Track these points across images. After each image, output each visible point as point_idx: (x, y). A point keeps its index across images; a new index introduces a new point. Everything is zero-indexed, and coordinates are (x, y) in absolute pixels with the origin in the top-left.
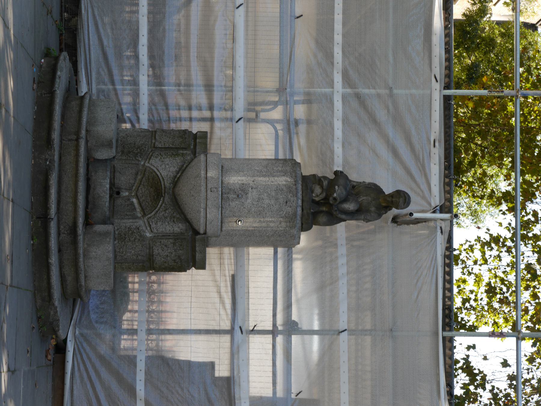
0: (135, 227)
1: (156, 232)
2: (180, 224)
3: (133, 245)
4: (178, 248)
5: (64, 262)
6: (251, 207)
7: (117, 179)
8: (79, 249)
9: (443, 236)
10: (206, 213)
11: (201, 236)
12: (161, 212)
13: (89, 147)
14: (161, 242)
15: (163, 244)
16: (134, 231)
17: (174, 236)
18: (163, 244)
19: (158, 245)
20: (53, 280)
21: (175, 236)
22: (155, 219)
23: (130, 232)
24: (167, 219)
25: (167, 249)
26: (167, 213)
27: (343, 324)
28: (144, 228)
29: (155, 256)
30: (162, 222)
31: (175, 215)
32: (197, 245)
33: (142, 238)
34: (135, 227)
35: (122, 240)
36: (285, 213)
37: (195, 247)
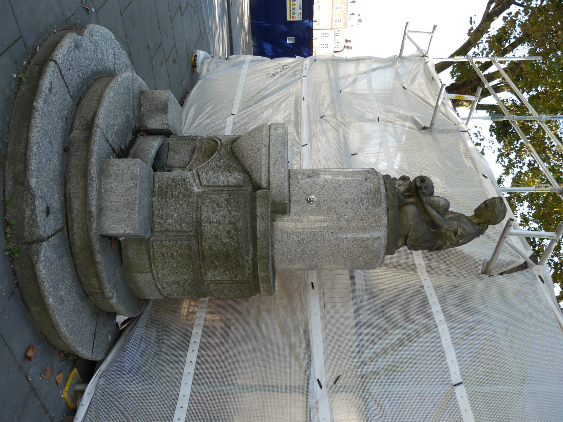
0: (180, 178)
1: (207, 184)
2: (236, 174)
3: (176, 204)
4: (234, 209)
5: (72, 170)
6: (324, 184)
7: (170, 158)
8: (93, 143)
9: (545, 284)
10: (269, 151)
11: (262, 190)
12: (214, 162)
13: (142, 113)
14: (211, 199)
15: (214, 202)
16: (179, 182)
17: (228, 190)
18: (214, 202)
19: (208, 202)
20: (33, 135)
21: (230, 191)
22: (206, 169)
23: (174, 184)
24: (221, 168)
26: (222, 163)
27: (456, 377)
28: (192, 181)
29: (203, 224)
30: (215, 172)
31: (231, 164)
32: (258, 204)
33: (189, 193)
34: (180, 178)
35: (163, 196)
36: (365, 188)
37: (255, 209)
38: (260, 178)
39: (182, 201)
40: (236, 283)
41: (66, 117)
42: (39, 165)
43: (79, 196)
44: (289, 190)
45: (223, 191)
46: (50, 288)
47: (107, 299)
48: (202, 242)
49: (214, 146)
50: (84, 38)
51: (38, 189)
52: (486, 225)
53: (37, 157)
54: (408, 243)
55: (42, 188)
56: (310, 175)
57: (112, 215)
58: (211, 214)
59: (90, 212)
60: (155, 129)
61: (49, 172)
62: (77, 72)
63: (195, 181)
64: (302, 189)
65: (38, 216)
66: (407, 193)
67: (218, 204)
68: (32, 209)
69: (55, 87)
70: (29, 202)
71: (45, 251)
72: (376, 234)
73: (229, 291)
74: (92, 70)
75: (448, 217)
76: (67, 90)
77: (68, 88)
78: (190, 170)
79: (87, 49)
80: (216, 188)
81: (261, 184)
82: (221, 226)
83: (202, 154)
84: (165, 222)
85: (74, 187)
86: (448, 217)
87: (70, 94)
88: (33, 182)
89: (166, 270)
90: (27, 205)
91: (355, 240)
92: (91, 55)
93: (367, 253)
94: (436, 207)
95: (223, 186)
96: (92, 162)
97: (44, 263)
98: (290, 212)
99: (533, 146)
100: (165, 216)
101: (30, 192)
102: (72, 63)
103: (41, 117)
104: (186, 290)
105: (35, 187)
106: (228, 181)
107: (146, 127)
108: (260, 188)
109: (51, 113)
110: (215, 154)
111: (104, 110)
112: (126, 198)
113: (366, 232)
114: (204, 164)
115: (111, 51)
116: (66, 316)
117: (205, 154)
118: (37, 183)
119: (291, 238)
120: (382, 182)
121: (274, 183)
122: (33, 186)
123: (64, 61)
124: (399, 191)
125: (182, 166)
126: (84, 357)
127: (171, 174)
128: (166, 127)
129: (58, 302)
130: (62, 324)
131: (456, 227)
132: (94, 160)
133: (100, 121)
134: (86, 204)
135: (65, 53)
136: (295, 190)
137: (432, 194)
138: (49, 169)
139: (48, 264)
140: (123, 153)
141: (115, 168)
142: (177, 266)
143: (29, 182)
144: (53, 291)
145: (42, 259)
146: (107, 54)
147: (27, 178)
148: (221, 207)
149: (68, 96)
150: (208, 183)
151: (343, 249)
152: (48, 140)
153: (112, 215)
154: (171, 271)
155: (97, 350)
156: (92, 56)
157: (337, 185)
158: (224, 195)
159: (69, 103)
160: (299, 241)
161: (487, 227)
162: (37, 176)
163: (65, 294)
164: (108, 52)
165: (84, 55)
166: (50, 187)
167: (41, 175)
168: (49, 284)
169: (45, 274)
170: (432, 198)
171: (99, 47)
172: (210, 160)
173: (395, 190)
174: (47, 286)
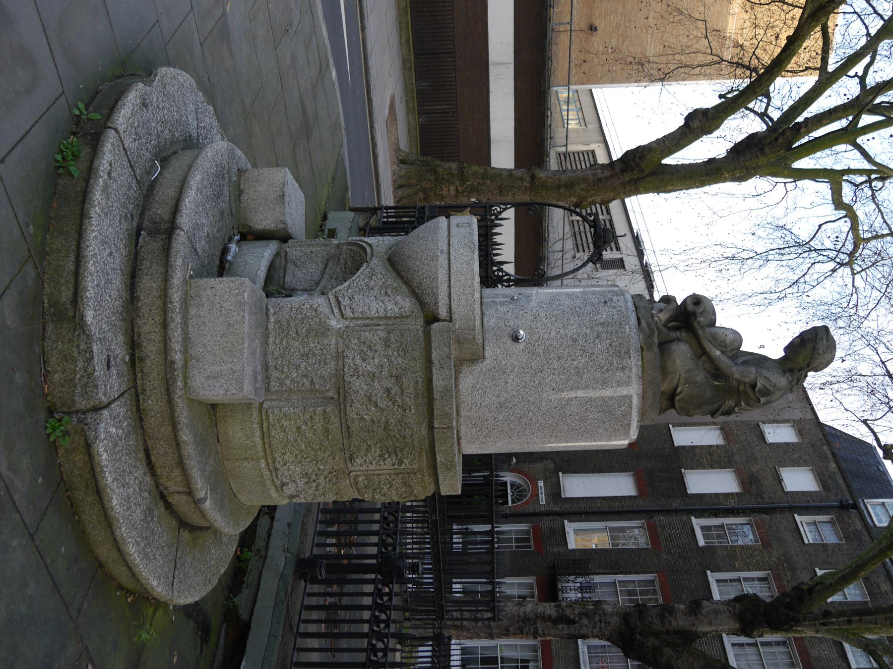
4: (395, 353)
10: (449, 260)
11: (441, 323)
14: (359, 338)
15: (364, 343)
19: (355, 344)
22: (350, 291)
25: (372, 354)
28: (327, 311)
33: (323, 331)
38: (436, 303)
39: (314, 343)
40: (400, 474)
41: (132, 216)
42: (96, 290)
43: (153, 337)
44: (482, 323)
45: (378, 325)
46: (113, 482)
47: (197, 503)
48: (345, 407)
49: (360, 256)
50: (153, 89)
51: (96, 328)
52: (803, 372)
53: (94, 277)
54: (677, 405)
55: (101, 326)
56: (516, 298)
57: (206, 367)
58: (358, 361)
59: (173, 362)
60: (264, 230)
61: (110, 300)
62: (146, 143)
63: (333, 311)
64: (503, 321)
65: (97, 368)
66: (672, 324)
67: (370, 347)
68: (86, 358)
69: (116, 170)
70: (83, 346)
71: (107, 424)
72: (623, 391)
73: (389, 488)
74: (166, 139)
75: (740, 360)
76: (132, 173)
77: (133, 170)
78: (323, 294)
79: (158, 107)
80: (367, 322)
81: (438, 314)
82: (376, 381)
83: (341, 269)
84: (287, 377)
85: (148, 326)
86: (740, 360)
87: (137, 179)
88: (89, 316)
89: (288, 454)
90: (79, 352)
91: (591, 400)
92: (164, 116)
93: (610, 420)
94: (722, 345)
95: (378, 318)
96: (173, 283)
97: (105, 442)
98: (484, 357)
99: (541, 258)
100: (286, 367)
101: (84, 332)
102: (139, 130)
103: (99, 215)
104: (176, 594)
105: (92, 323)
106: (385, 310)
107: (250, 227)
108: (436, 319)
109: (110, 209)
110: (363, 268)
111: (190, 202)
112: (227, 340)
113: (607, 386)
114: (346, 284)
115: (192, 107)
116: (136, 528)
117: (345, 268)
118: (94, 317)
119: (487, 399)
120: (630, 305)
121: (459, 310)
122: (89, 323)
123: (127, 128)
124: (660, 320)
125: (309, 288)
126: (161, 597)
127: (295, 300)
128: (281, 226)
129: (124, 506)
130: (130, 540)
131: (753, 376)
132: (177, 279)
133: (185, 220)
134: (166, 350)
135: (128, 115)
136: (491, 322)
137: (713, 323)
138: (110, 296)
139: (110, 444)
140: (222, 268)
141: (209, 292)
142: (306, 447)
143: (83, 316)
144: (118, 487)
145: (103, 436)
146: (187, 113)
147: (79, 310)
148: (376, 351)
149: (134, 182)
150: (353, 313)
151: (571, 415)
152: (108, 251)
153: (206, 367)
154: (296, 455)
155: (180, 587)
156: (166, 117)
157: (558, 313)
158: (379, 332)
159: (135, 192)
160: (500, 403)
161: (806, 376)
162: (94, 306)
163: (133, 494)
164: (187, 110)
165: (154, 116)
166: (111, 325)
167: (101, 306)
168: (112, 476)
169: (106, 460)
170: (712, 330)
171: (175, 102)
172: (355, 276)
173: (652, 317)
174: (109, 479)
